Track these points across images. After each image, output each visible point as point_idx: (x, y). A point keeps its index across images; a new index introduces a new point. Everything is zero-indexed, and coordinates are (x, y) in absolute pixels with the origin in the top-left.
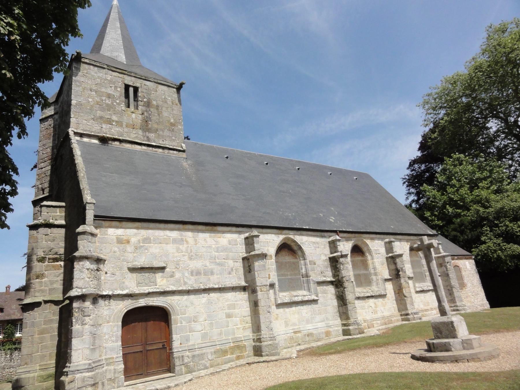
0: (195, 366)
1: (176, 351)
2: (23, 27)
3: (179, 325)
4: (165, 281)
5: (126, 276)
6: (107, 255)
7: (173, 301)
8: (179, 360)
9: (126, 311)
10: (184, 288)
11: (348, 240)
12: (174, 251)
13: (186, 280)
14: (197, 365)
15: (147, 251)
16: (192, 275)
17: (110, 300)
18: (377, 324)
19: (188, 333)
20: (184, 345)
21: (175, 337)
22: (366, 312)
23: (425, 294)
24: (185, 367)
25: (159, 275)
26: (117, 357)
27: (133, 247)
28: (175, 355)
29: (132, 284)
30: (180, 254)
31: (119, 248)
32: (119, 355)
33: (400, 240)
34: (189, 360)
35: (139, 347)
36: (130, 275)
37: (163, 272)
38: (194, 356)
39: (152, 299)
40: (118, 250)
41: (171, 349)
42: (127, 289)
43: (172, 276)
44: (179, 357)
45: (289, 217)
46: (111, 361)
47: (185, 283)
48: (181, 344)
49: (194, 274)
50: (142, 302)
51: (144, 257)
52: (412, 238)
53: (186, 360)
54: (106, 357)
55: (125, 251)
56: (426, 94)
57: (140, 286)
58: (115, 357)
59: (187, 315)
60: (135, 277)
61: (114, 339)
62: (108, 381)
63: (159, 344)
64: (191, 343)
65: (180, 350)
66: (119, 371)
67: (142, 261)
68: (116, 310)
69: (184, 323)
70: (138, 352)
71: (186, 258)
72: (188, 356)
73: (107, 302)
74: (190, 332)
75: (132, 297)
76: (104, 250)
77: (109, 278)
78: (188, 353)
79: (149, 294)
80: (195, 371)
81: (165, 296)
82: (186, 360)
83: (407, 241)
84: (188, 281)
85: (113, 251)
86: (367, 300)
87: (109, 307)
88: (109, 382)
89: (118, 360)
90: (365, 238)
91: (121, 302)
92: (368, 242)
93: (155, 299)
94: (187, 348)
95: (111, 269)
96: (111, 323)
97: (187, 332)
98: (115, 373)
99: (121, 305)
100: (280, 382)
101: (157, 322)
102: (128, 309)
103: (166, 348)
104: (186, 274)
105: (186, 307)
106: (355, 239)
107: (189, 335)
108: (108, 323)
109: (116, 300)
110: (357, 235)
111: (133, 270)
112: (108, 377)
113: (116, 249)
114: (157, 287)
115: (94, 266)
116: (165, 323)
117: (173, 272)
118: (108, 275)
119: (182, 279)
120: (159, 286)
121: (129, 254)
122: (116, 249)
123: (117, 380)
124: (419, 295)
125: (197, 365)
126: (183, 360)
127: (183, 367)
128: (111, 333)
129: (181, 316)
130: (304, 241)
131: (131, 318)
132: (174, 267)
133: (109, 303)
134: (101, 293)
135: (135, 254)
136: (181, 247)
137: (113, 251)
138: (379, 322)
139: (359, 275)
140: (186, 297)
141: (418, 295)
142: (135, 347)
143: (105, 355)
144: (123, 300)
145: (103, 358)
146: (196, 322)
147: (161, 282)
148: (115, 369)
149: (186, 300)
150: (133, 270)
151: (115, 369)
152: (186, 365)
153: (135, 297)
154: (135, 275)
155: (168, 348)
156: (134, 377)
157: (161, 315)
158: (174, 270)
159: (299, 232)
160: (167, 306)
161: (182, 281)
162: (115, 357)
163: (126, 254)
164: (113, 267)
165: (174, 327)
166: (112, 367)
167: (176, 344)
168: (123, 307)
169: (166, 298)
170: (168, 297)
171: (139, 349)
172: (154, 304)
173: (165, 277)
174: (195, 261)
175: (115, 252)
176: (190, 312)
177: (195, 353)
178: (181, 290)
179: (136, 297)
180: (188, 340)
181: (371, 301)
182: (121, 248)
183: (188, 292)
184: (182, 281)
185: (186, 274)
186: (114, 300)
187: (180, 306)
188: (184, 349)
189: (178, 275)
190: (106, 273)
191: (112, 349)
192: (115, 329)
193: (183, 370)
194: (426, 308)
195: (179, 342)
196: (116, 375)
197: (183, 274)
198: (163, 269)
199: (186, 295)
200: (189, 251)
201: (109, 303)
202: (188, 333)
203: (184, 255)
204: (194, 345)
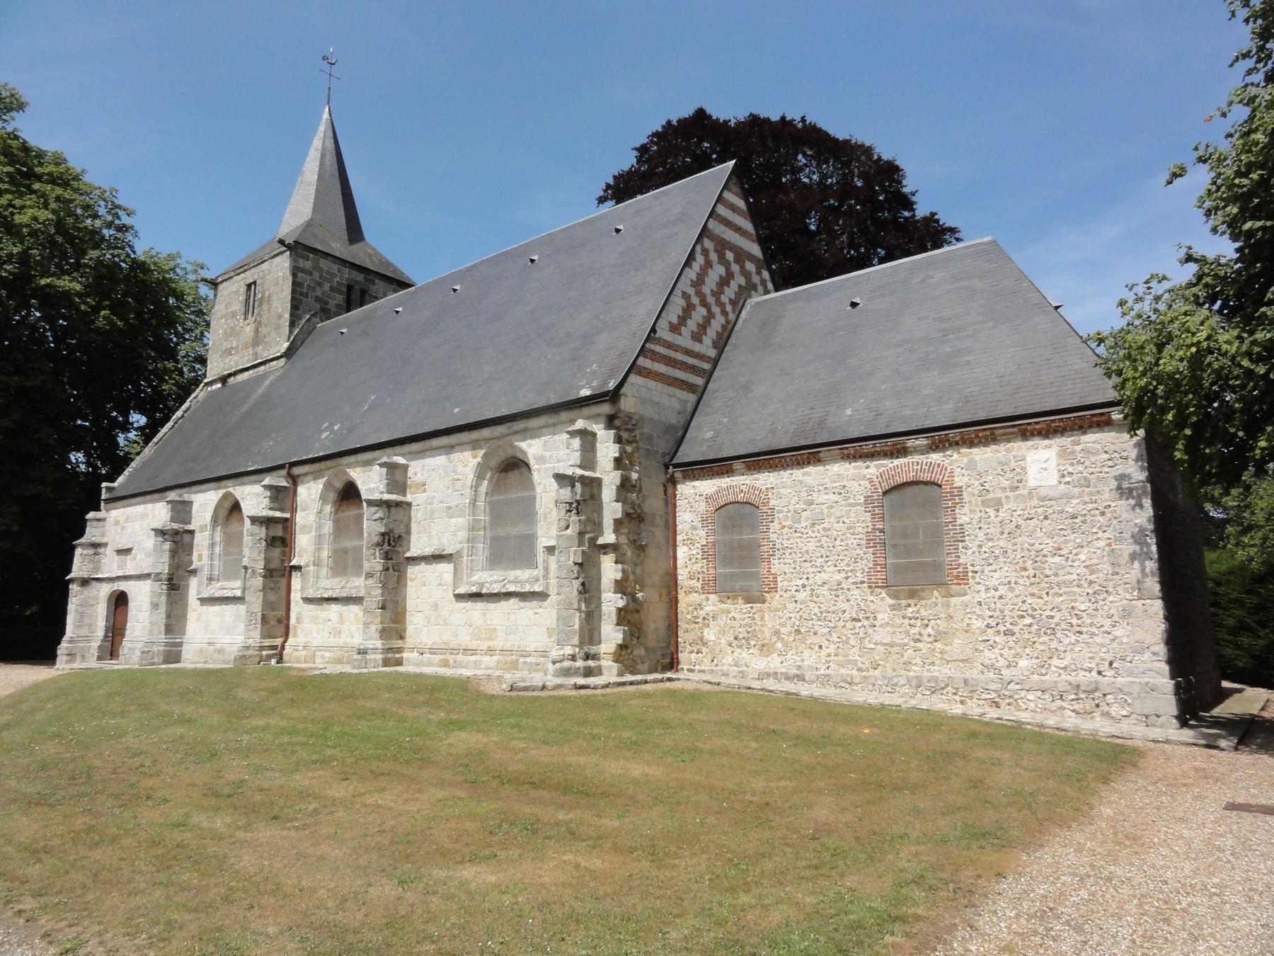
2: (67, 295)
11: (317, 475)
18: (323, 657)
22: (318, 631)
23: (492, 606)
33: (421, 454)
45: (324, 443)
52: (486, 432)
56: (1244, 73)
83: (475, 445)
86: (326, 606)
90: (349, 466)
92: (523, 445)
106: (330, 472)
110: (329, 463)
115: (91, 551)
124: (469, 605)
130: (532, 448)
138: (327, 654)
139: (345, 551)
141: (462, 605)
159: (240, 480)
181: (335, 608)
194: (473, 644)
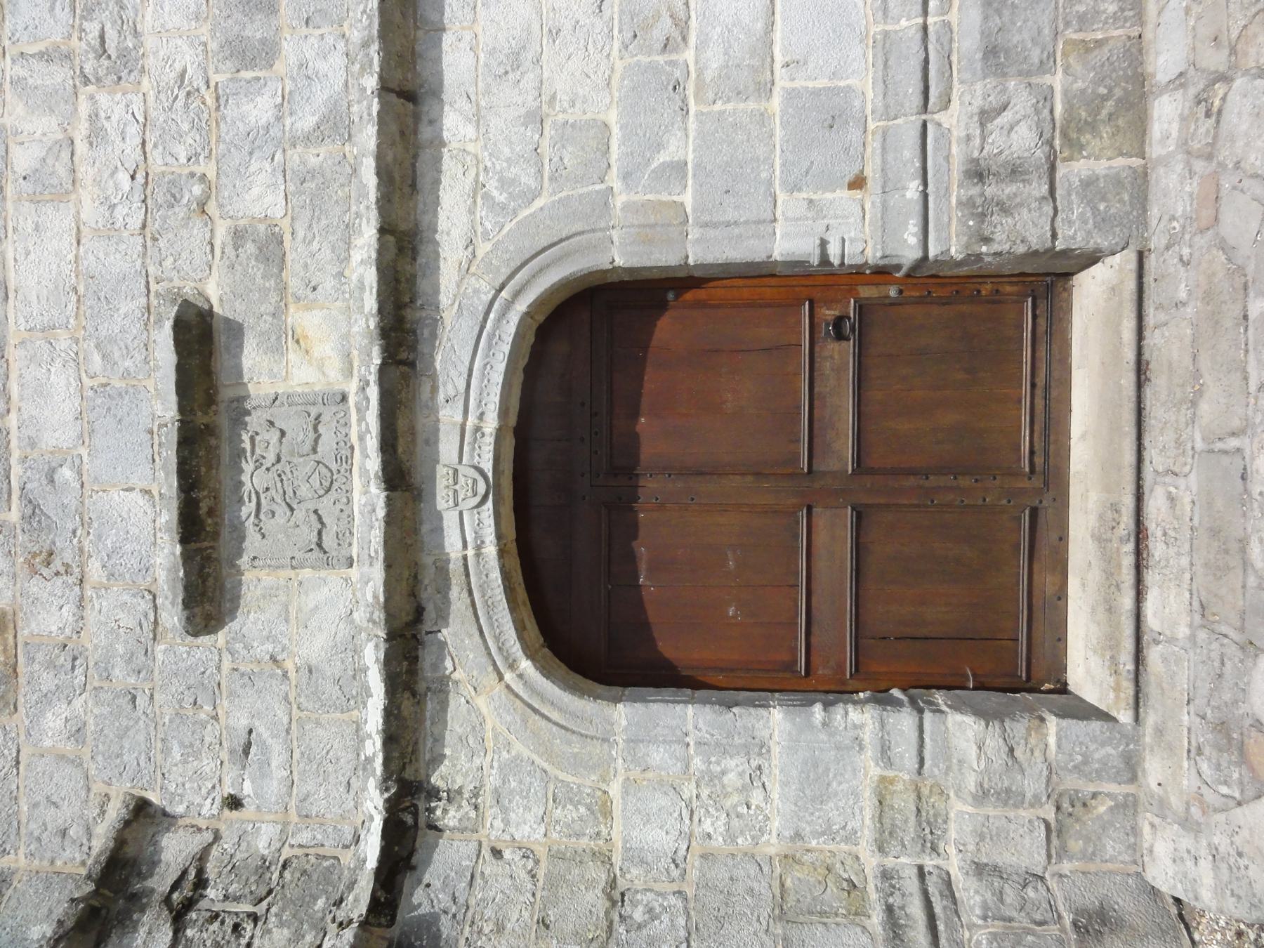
0: (1086, 48)
1: (911, 236)
3: (688, 199)
4: (306, 320)
5: (263, 650)
6: (98, 787)
7: (483, 248)
8: (1005, 209)
9: (526, 665)
10: (368, 137)
12: (59, 220)
13: (306, 121)
14: (1084, 21)
15: (66, 473)
16: (266, 53)
17: (434, 794)
19: (776, 103)
20: (874, 145)
21: (788, 242)
24: (1075, 147)
25: (260, 372)
26: (885, 753)
27: (35, 586)
28: (950, 243)
29: (315, 606)
30: (86, 172)
31: (46, 699)
32: (868, 735)
34: (1022, 102)
35: (821, 538)
36: (252, 622)
37: (236, 330)
38: (995, 56)
39: (447, 449)
40: (62, 709)
41: (882, 273)
42: (357, 651)
43: (271, 250)
44: (979, 211)
46: (904, 802)
47: (335, 125)
48: (858, 183)
49: (255, 30)
50: (469, 529)
51: (116, 496)
53: (1021, 140)
54: (867, 834)
55: (69, 653)
57: (344, 537)
58: (875, 771)
59: (613, 117)
60: (267, 578)
61: (734, 769)
62: (1063, 853)
63: (826, 367)
64: (864, 83)
65: (913, 190)
66: (1000, 759)
67: (138, 513)
68: (518, 747)
69: (681, 146)
70: (859, 549)
71: (114, 106)
72: (985, 116)
73: (449, 817)
74: (766, 89)
75: (419, 612)
76: (67, 812)
77: (274, 787)
78: (954, 120)
79: (403, 477)
80: (1136, 49)
81: (436, 322)
82: (1021, 140)
84: (321, 96)
85: (69, 748)
87: (486, 799)
88: (1075, 845)
89: (905, 752)
91: (456, 706)
93: (449, 416)
94: (908, 127)
95: (207, 765)
96: (615, 789)
97: (762, 118)
98: (1009, 797)
99: (481, 702)
100: (558, 302)
101: (652, 381)
102: (516, 649)
103: (862, 308)
104: (259, 110)
105: (536, 119)
107: (791, 95)
108: (607, 813)
109: (439, 740)
111: (207, 594)
112: (1027, 851)
113: (54, 721)
114: (352, 388)
116: (663, 306)
117: (238, 236)
118: (248, 788)
119: (294, 155)
120: (348, 372)
121: (91, 616)
122: (54, 721)
123: (1071, 782)
125: (1084, 21)
126: (1015, 171)
127: (1073, 171)
128: (689, 790)
129: (614, 179)
131: (595, 629)
132: (198, 230)
133: (453, 796)
134: (358, 903)
135: (95, 570)
136: (23, 159)
137: (69, 748)
140: (455, 124)
142: (821, 565)
143: (852, 838)
144: (442, 687)
145: (871, 861)
146: (682, 25)
147: (311, 357)
148: (982, 795)
149: (478, 119)
150: (207, 594)
151: (982, 795)
152: (1064, 137)
153: (427, 595)
154: (256, 583)
155: (866, 292)
156: (1047, 582)
157: (600, 338)
158: (222, 232)
160: (521, 306)
161: (317, 156)
162: (875, 771)
163: (94, 640)
164: (191, 752)
165: (699, 249)
166: (961, 816)
167: (852, 227)
168: (493, 684)
169: (448, 316)
170: (444, 299)
171: (834, 533)
172: (491, 424)
173: (278, 313)
174: (147, 23)
175: (78, 733)
176: (588, 78)
177: (967, 44)
178: (383, 172)
179: (428, 577)
180: (830, 112)
182: (47, 681)
183: (407, 94)
184: (317, 156)
185: (259, 110)
186: (438, 759)
187: (528, 180)
188: (910, 152)
189: (260, 196)
190: (234, 803)
191: (815, 784)
192: (657, 756)
193: (1101, 167)
195: (843, 194)
196: (1032, 785)
197: (256, 140)
198: (200, 341)
199: (435, 122)
200: (59, 75)
201: (453, 796)
202: (776, 103)
203: (96, 135)
204: (886, 46)
